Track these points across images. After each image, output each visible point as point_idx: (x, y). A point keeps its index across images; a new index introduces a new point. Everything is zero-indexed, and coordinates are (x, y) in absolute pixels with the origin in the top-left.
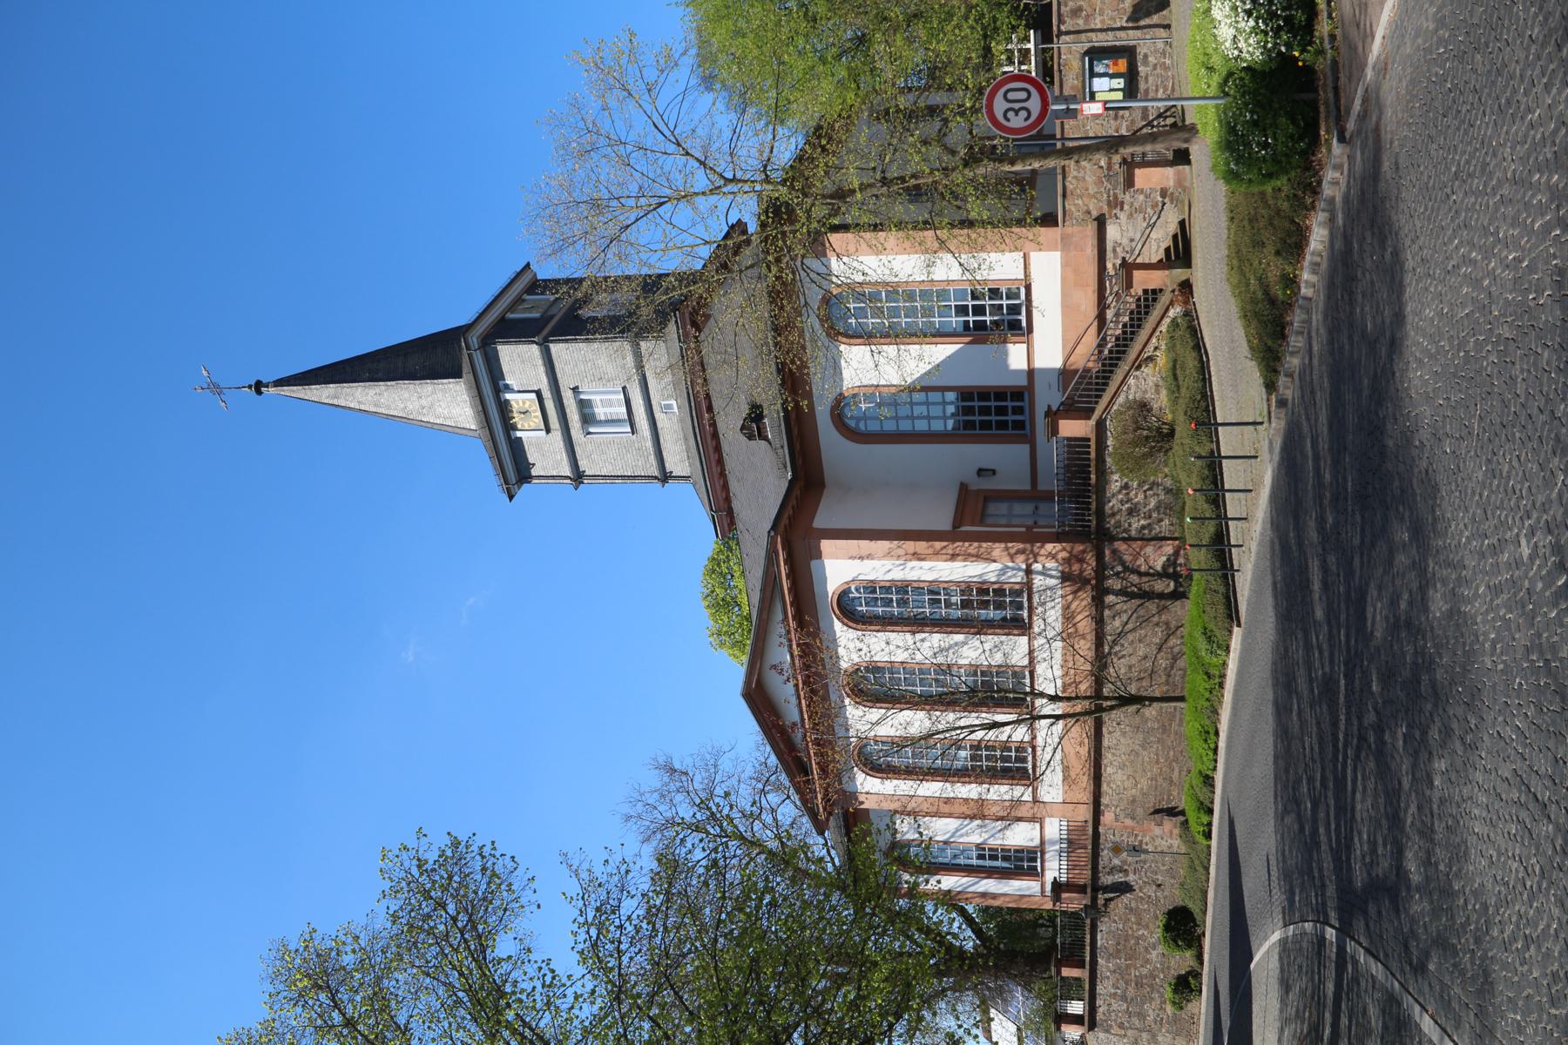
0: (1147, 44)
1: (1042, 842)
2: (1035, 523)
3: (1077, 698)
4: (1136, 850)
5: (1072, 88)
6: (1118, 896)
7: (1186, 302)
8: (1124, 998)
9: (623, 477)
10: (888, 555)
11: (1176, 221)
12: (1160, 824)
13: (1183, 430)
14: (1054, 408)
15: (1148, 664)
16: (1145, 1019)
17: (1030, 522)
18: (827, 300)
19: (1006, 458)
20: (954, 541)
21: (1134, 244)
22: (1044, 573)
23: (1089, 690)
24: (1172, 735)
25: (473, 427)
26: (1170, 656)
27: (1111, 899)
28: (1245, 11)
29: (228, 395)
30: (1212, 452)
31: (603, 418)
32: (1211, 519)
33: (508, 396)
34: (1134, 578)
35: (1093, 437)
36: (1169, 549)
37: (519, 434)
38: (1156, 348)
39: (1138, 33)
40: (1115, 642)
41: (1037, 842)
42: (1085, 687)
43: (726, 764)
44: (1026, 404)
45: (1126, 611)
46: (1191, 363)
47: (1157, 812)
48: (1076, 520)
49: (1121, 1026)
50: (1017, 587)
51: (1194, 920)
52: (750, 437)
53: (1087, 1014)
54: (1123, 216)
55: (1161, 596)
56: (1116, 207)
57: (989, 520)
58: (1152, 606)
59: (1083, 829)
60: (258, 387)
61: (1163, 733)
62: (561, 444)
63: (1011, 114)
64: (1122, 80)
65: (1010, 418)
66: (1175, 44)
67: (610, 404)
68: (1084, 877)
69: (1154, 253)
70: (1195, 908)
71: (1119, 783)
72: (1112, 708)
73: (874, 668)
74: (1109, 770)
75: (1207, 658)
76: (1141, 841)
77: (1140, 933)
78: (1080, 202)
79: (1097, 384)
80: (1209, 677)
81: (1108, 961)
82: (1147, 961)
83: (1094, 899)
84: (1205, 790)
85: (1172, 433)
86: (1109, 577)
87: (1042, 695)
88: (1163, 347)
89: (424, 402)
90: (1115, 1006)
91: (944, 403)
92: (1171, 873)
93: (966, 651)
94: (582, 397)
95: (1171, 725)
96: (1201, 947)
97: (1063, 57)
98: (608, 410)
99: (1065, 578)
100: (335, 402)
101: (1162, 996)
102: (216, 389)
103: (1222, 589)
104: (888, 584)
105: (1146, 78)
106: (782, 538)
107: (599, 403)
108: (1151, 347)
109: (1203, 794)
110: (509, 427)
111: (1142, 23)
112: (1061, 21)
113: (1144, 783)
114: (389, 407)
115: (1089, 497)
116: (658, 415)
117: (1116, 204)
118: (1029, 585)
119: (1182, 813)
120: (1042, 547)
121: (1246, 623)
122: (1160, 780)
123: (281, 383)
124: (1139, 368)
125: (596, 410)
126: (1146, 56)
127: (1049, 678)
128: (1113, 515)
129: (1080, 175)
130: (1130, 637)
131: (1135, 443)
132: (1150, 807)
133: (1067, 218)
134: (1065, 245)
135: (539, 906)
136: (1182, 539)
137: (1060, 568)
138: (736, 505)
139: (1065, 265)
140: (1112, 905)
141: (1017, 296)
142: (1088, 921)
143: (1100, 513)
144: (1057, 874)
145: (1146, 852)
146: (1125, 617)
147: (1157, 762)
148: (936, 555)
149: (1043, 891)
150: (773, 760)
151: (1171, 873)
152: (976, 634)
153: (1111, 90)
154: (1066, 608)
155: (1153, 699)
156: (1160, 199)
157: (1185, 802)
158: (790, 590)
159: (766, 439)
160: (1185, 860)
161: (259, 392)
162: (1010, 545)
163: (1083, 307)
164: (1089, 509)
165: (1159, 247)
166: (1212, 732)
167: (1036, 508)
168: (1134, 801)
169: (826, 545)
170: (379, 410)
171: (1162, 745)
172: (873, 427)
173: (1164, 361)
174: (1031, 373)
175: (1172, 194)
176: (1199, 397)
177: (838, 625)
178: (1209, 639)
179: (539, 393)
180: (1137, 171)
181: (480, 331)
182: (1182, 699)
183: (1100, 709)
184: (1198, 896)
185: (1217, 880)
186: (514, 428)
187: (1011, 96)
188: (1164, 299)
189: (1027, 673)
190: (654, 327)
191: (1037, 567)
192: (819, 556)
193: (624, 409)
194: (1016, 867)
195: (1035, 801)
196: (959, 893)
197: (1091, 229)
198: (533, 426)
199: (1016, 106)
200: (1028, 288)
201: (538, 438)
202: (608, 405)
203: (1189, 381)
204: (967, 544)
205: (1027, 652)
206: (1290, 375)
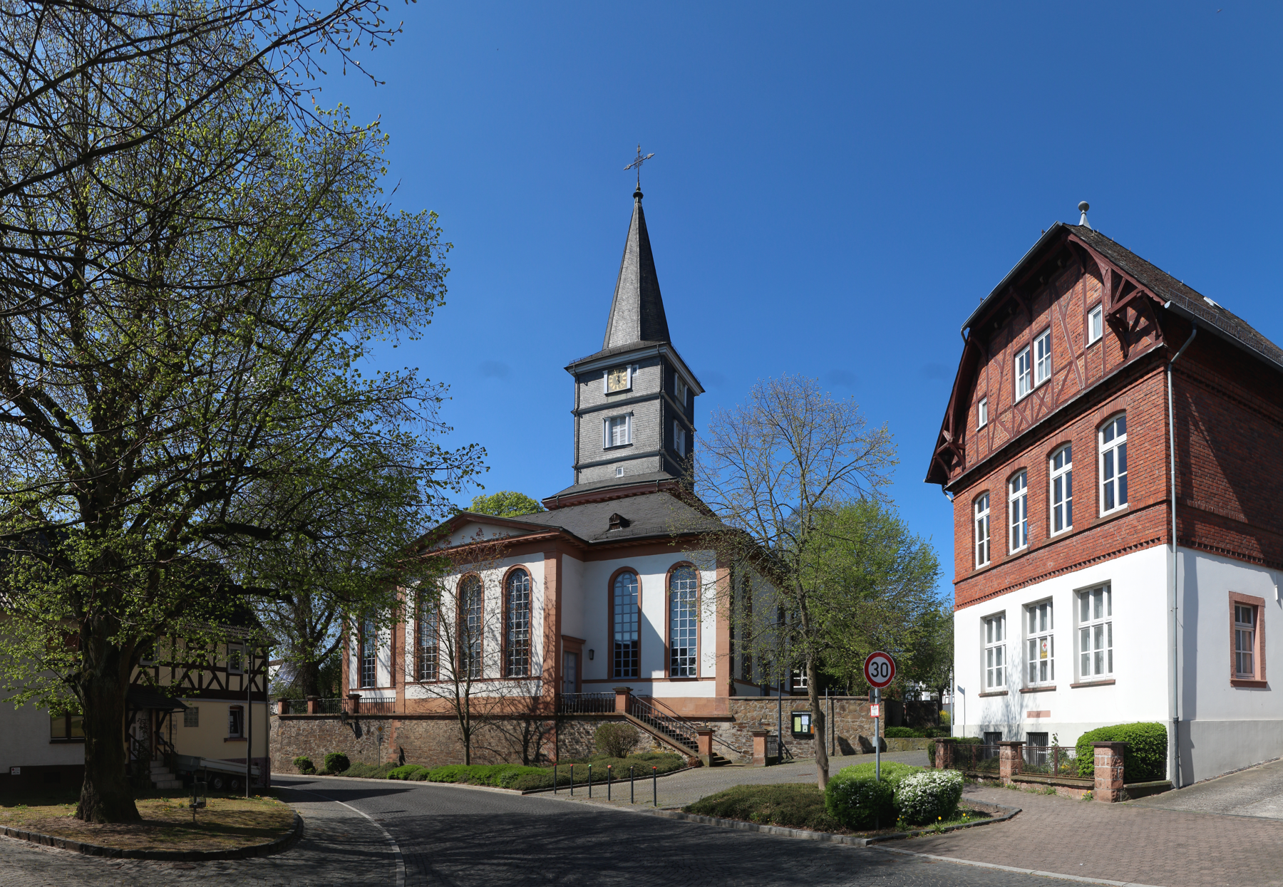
1: (379, 689)
4: (381, 739)
7: (691, 764)
8: (298, 734)
9: (578, 442)
10: (547, 598)
12: (395, 752)
13: (623, 763)
17: (565, 679)
18: (688, 565)
19: (600, 666)
20: (556, 635)
33: (629, 370)
34: (535, 738)
35: (615, 713)
36: (552, 756)
37: (606, 376)
40: (498, 727)
44: (630, 677)
46: (662, 767)
49: (283, 733)
52: (611, 519)
55: (525, 751)
58: (519, 748)
59: (389, 710)
60: (639, 195)
63: (875, 666)
65: (622, 669)
67: (623, 435)
69: (717, 748)
70: (350, 770)
73: (480, 591)
74: (424, 724)
82: (318, 746)
83: (351, 718)
85: (621, 756)
86: (536, 723)
87: (469, 687)
89: (626, 313)
91: (631, 632)
92: (368, 758)
93: (493, 644)
96: (328, 774)
98: (619, 434)
99: (535, 699)
102: (639, 163)
103: (542, 784)
108: (666, 745)
110: (610, 370)
112: (838, 700)
113: (417, 743)
114: (623, 289)
116: (615, 466)
117: (741, 727)
118: (530, 678)
124: (654, 739)
127: (478, 690)
131: (617, 737)
132: (405, 747)
134: (719, 700)
135: (395, 346)
136: (557, 762)
138: (566, 510)
139: (708, 700)
140: (348, 727)
141: (691, 673)
143: (573, 718)
149: (352, 690)
151: (368, 758)
155: (468, 747)
157: (408, 766)
159: (610, 529)
160: (375, 766)
161: (636, 195)
169: (553, 562)
172: (618, 591)
174: (650, 680)
177: (505, 569)
178: (511, 778)
179: (630, 390)
180: (763, 739)
182: (468, 763)
183: (462, 718)
184: (357, 773)
186: (609, 374)
187: (884, 666)
188: (692, 753)
190: (666, 467)
192: (547, 557)
193: (619, 444)
195: (406, 684)
197: (727, 714)
198: (611, 385)
200: (696, 680)
202: (623, 434)
203: (652, 766)
206: (702, 820)
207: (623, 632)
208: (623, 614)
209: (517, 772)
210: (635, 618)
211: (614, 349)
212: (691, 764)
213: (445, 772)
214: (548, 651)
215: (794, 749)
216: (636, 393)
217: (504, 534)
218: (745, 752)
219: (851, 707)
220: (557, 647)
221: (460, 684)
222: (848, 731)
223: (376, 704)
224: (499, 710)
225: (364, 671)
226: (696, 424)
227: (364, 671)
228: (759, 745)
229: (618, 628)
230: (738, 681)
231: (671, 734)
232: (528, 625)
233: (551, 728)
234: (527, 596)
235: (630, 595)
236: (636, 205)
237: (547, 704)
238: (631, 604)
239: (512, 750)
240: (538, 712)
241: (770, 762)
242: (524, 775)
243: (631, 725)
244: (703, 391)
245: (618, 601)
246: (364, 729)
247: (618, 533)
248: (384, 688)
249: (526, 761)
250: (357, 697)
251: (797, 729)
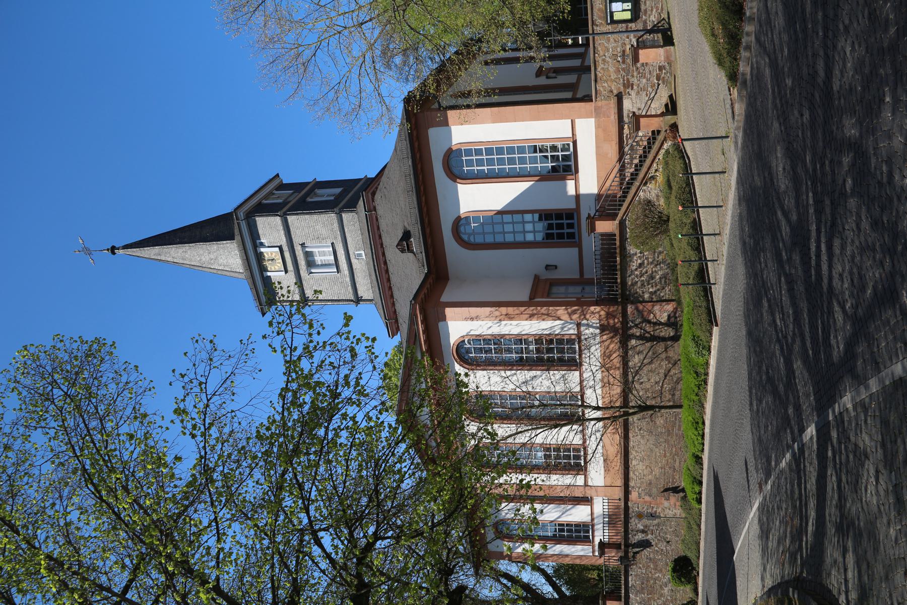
1: (592, 519)
4: (653, 516)
5: (599, 10)
6: (642, 550)
7: (675, 138)
10: (488, 317)
11: (667, 96)
12: (668, 499)
15: (658, 388)
17: (580, 296)
24: (674, 437)
25: (241, 271)
30: (695, 219)
31: (320, 263)
32: (695, 261)
33: (262, 250)
34: (648, 328)
35: (617, 233)
36: (670, 307)
37: (269, 274)
38: (656, 170)
40: (637, 373)
41: (588, 519)
44: (575, 221)
47: (666, 490)
51: (691, 564)
52: (403, 251)
54: (633, 93)
55: (664, 339)
56: (628, 88)
58: (660, 347)
59: (618, 507)
60: (113, 250)
61: (668, 435)
65: (566, 231)
67: (324, 254)
68: (619, 539)
70: (691, 555)
71: (641, 471)
77: (657, 575)
80: (697, 376)
81: (636, 595)
82: (662, 595)
83: (626, 552)
84: (697, 467)
86: (631, 328)
87: (590, 407)
88: (661, 170)
89: (212, 256)
91: (524, 222)
92: (675, 533)
94: (307, 250)
95: (673, 430)
96: (696, 584)
98: (323, 258)
99: (603, 328)
100: (159, 258)
102: (88, 251)
103: (704, 304)
104: (489, 337)
106: (420, 307)
107: (317, 254)
110: (263, 269)
113: (657, 471)
114: (191, 260)
115: (616, 274)
116: (354, 261)
117: (628, 85)
118: (579, 335)
119: (683, 490)
121: (721, 324)
123: (126, 247)
124: (646, 184)
127: (591, 398)
129: (606, 67)
132: (661, 487)
133: (598, 95)
134: (598, 114)
139: (598, 126)
141: (568, 150)
143: (624, 283)
144: (602, 538)
149: (593, 552)
151: (675, 533)
153: (624, 10)
156: (656, 82)
157: (684, 482)
159: (412, 252)
161: (114, 253)
163: (610, 155)
164: (616, 283)
166: (700, 423)
167: (583, 289)
168: (650, 484)
169: (449, 311)
170: (185, 262)
172: (479, 239)
173: (661, 179)
174: (578, 197)
175: (664, 78)
179: (280, 248)
180: (641, 52)
182: (680, 407)
183: (626, 414)
184: (694, 547)
185: (706, 532)
188: (660, 138)
190: (351, 206)
192: (444, 318)
193: (332, 258)
195: (586, 485)
197: (613, 102)
200: (575, 143)
201: (280, 276)
202: (323, 255)
204: (539, 308)
206: (748, 48)
207: (524, 232)
208: (504, 233)
209: (691, 337)
210: (507, 218)
211: (245, 267)
212: (675, 138)
213: (691, 433)
214: (548, 315)
215: (652, 18)
216: (283, 241)
218: (658, 79)
220: (543, 304)
221: (587, 416)
223: (609, 523)
224: (617, 372)
225: (571, 537)
226: (308, 179)
227: (571, 537)
228: (652, 56)
229: (519, 238)
230: (575, 93)
231: (638, 168)
232: (520, 339)
233: (637, 309)
234: (487, 341)
235: (483, 224)
236: (121, 252)
237: (609, 315)
238: (493, 224)
239: (663, 356)
240: (618, 325)
241: (668, 41)
242: (694, 328)
243: (632, 216)
244: (278, 175)
245: (489, 239)
246: (640, 537)
247: (416, 243)
248: (592, 514)
249: (676, 338)
250: (602, 545)
251: (627, 15)
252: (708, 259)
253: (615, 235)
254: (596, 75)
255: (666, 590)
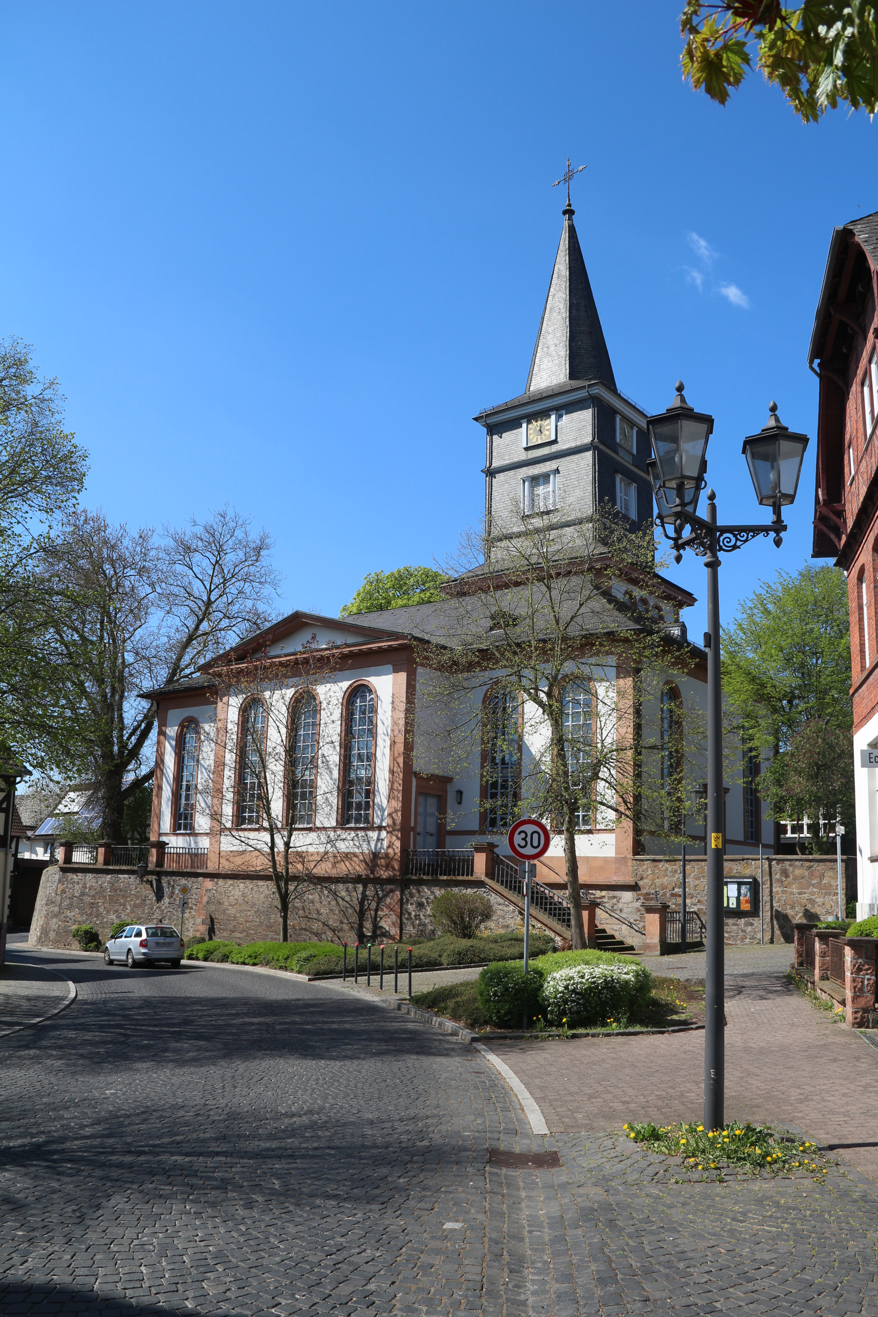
0: (760, 925)
2: (419, 834)
3: (287, 863)
5: (731, 869)
8: (83, 894)
10: (395, 723)
11: (633, 944)
12: (203, 923)
14: (496, 850)
16: (68, 909)
17: (419, 829)
21: (618, 912)
22: (379, 839)
23: (295, 871)
24: (264, 933)
25: (532, 388)
26: (320, 932)
27: (152, 886)
28: (568, 985)
29: (564, 187)
33: (553, 417)
34: (374, 905)
36: (394, 931)
37: (524, 425)
39: (768, 919)
42: (297, 868)
43: (267, 590)
45: (352, 900)
48: (417, 864)
49: (63, 892)
50: (370, 819)
53: (72, 866)
55: (361, 926)
56: (645, 899)
57: (421, 799)
58: (355, 918)
60: (569, 212)
61: (267, 926)
62: (516, 460)
63: (523, 835)
64: (735, 906)
66: (758, 947)
72: (279, 887)
74: (242, 885)
75: (296, 958)
76: (192, 908)
77: (128, 907)
78: (649, 872)
79: (511, 882)
81: (109, 882)
82: (108, 912)
83: (152, 873)
88: (534, 932)
89: (552, 348)
90: (77, 887)
94: (552, 477)
97: (753, 862)
99: (375, 855)
100: (555, 276)
101: (84, 922)
102: (568, 177)
104: (374, 722)
105: (736, 925)
106: (406, 644)
109: (217, 954)
110: (531, 417)
111: (775, 922)
112: (779, 861)
113: (232, 911)
114: (549, 320)
115: (432, 875)
118: (372, 829)
119: (211, 939)
120: (398, 838)
122: (234, 923)
123: (572, 230)
125: (542, 487)
126: (752, 924)
127: (302, 841)
128: (419, 892)
130: (333, 903)
132: (217, 916)
134: (620, 860)
137: (382, 851)
139: (606, 860)
142: (136, 868)
143: (421, 882)
145: (183, 913)
146: (348, 899)
147: (246, 921)
148: (394, 759)
150: (268, 625)
152: (338, 787)
153: (728, 898)
154: (355, 855)
155: (285, 918)
158: (370, 649)
159: (492, 629)
161: (565, 213)
162: (399, 814)
165: (616, 931)
166: (256, 961)
167: (431, 835)
168: (220, 903)
169: (403, 676)
171: (258, 925)
176: (482, 956)
178: (307, 959)
179: (555, 442)
180: (657, 916)
181: (604, 395)
182: (285, 939)
186: (529, 422)
187: (535, 836)
189: (310, 826)
191: (384, 834)
192: (396, 671)
194: (180, 815)
196: (162, 771)
197: (629, 880)
199: (528, 839)
200: (590, 832)
204: (401, 782)
205: (326, 826)
216: (561, 447)
217: (351, 640)
219: (798, 872)
222: (793, 907)
232: (371, 758)
252: (399, 975)
253: (472, 875)
254: (660, 861)
255: (113, 917)
